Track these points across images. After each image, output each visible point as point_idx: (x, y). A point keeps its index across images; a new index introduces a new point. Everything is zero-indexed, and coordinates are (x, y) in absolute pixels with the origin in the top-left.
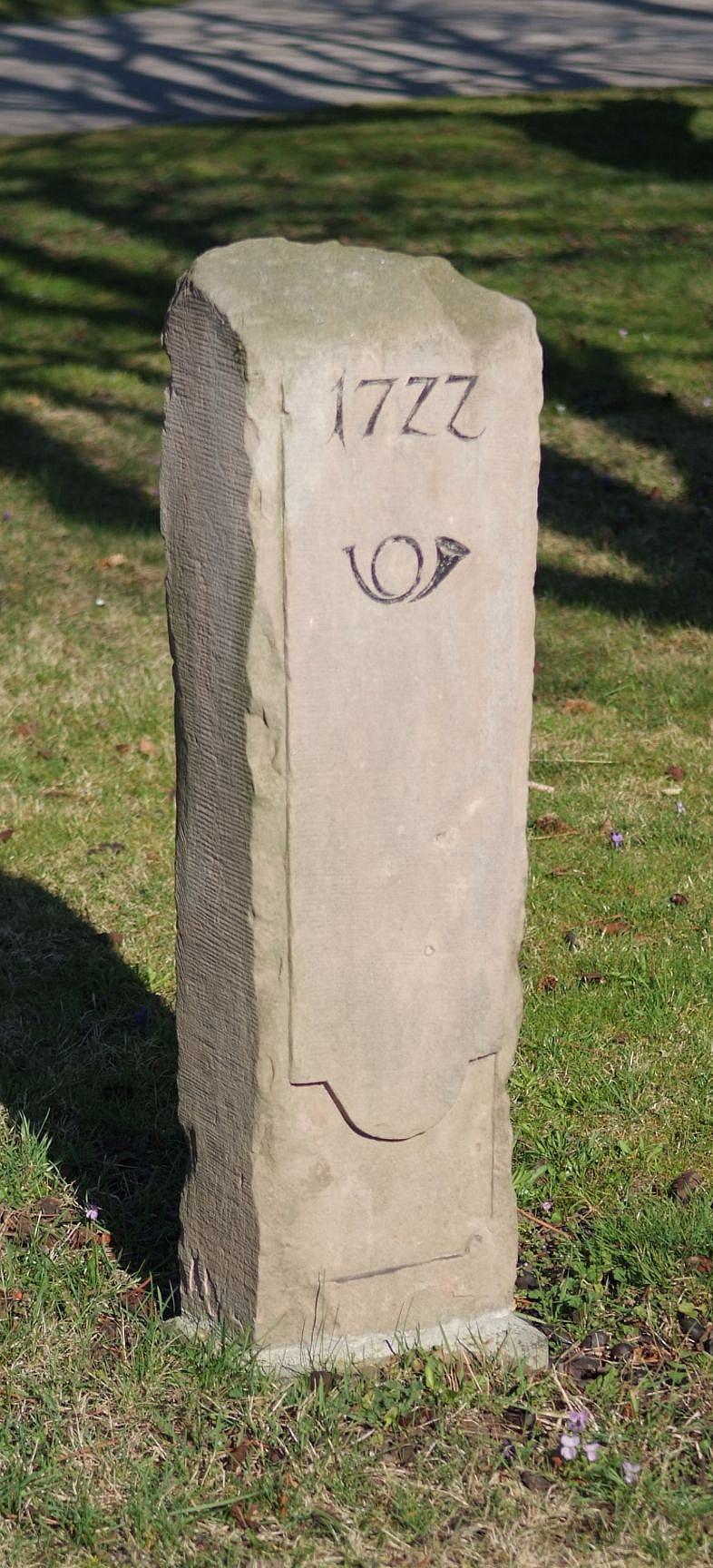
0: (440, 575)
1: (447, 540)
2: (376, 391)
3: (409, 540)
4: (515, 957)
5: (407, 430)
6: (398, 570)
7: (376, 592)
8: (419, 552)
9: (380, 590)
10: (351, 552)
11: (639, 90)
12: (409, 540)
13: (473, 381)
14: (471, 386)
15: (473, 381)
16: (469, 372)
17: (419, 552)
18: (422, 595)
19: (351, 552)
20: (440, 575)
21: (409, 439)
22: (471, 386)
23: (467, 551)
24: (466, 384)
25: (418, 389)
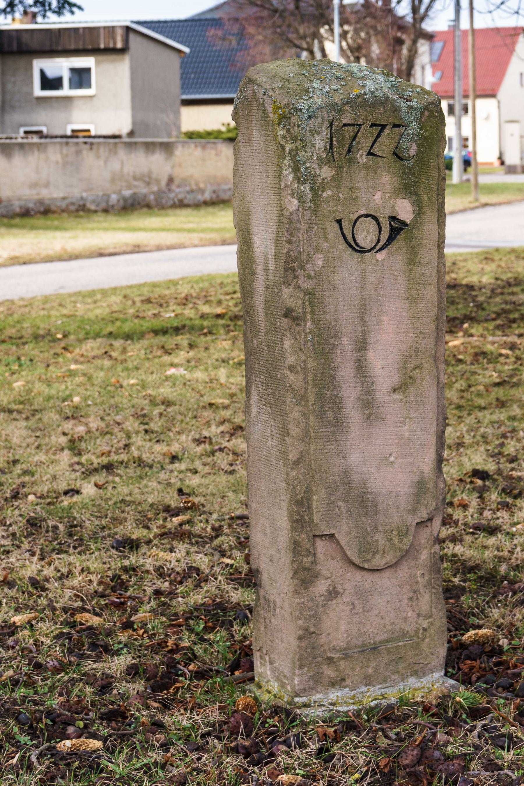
0: (391, 239)
5: (370, 154)
7: (355, 247)
10: (339, 222)
18: (380, 250)
19: (339, 222)
20: (391, 239)
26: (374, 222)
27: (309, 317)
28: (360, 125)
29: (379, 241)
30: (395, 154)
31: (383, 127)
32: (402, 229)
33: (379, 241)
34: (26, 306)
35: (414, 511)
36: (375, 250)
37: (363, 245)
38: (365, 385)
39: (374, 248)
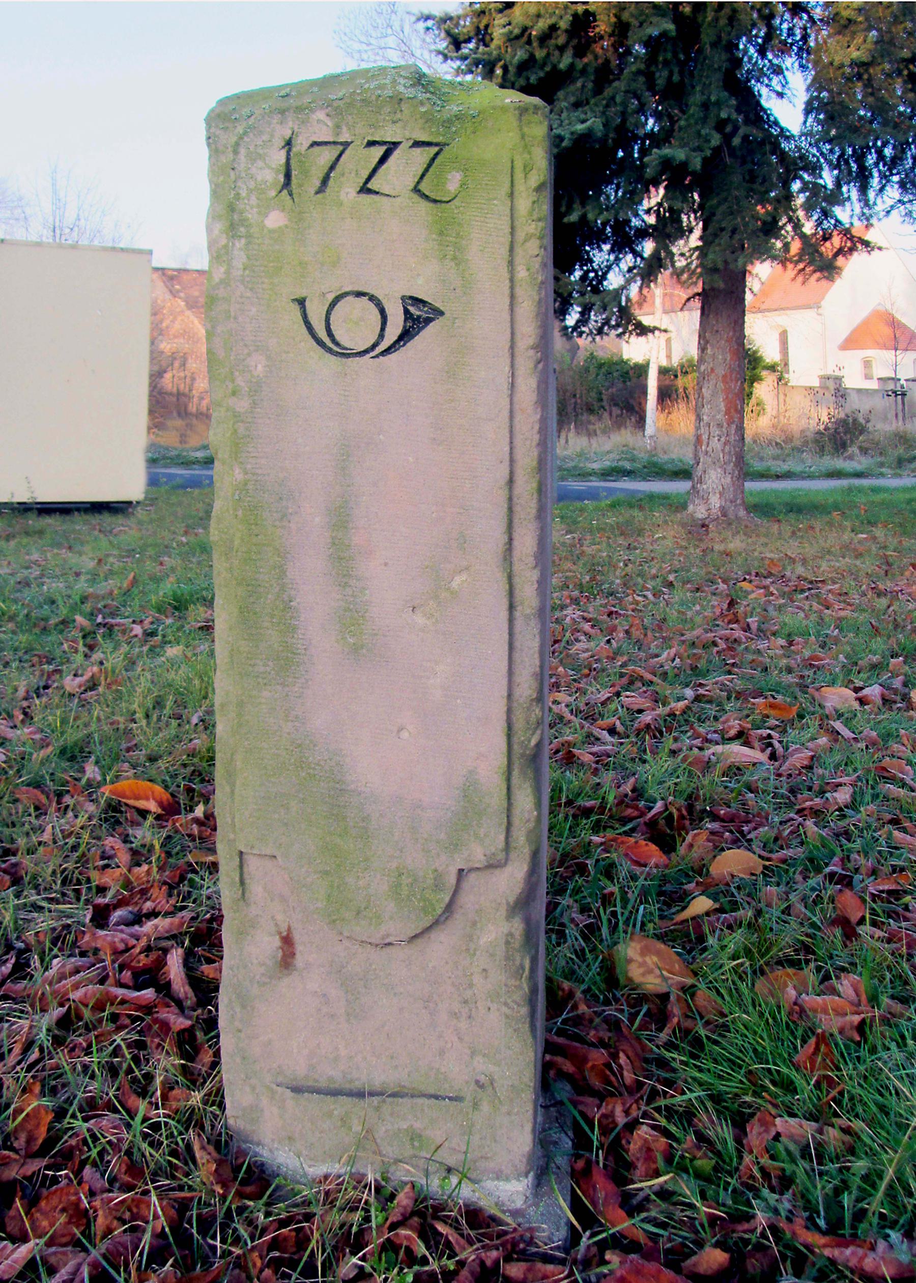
0: (405, 336)
1: (417, 301)
2: (326, 156)
3: (372, 298)
4: (449, 922)
5: (365, 190)
6: (356, 326)
7: (330, 345)
8: (382, 312)
9: (337, 344)
10: (301, 302)
11: (762, 492)
12: (372, 298)
13: (441, 146)
14: (383, 160)
15: (441, 146)
16: (440, 139)
17: (382, 312)
18: (387, 351)
19: (301, 302)
20: (405, 336)
21: (367, 198)
22: (383, 160)
23: (442, 313)
24: (436, 149)
25: (379, 151)
26: (372, 306)
27: (822, 160)
28: (346, 145)
29: (381, 336)
30: (416, 190)
31: (392, 147)
32: (428, 321)
33: (381, 336)
34: (582, 1142)
35: (454, 846)
36: (372, 354)
37: (345, 342)
38: (349, 591)
39: (374, 346)
